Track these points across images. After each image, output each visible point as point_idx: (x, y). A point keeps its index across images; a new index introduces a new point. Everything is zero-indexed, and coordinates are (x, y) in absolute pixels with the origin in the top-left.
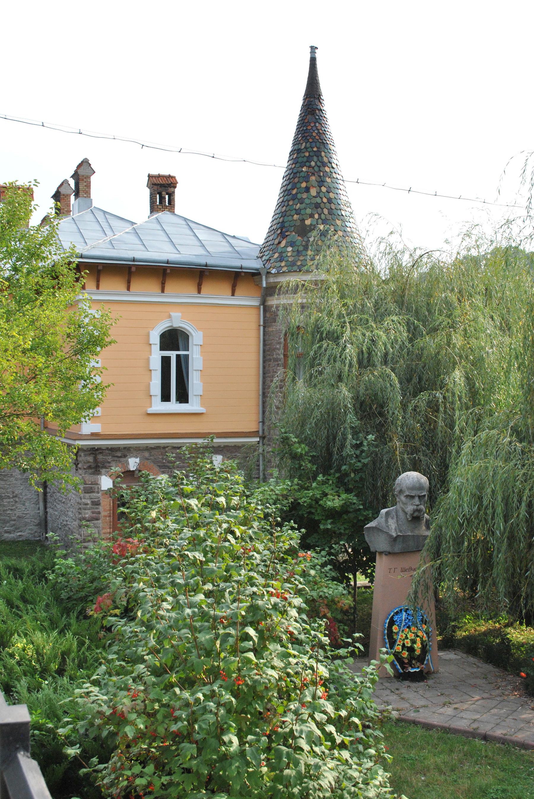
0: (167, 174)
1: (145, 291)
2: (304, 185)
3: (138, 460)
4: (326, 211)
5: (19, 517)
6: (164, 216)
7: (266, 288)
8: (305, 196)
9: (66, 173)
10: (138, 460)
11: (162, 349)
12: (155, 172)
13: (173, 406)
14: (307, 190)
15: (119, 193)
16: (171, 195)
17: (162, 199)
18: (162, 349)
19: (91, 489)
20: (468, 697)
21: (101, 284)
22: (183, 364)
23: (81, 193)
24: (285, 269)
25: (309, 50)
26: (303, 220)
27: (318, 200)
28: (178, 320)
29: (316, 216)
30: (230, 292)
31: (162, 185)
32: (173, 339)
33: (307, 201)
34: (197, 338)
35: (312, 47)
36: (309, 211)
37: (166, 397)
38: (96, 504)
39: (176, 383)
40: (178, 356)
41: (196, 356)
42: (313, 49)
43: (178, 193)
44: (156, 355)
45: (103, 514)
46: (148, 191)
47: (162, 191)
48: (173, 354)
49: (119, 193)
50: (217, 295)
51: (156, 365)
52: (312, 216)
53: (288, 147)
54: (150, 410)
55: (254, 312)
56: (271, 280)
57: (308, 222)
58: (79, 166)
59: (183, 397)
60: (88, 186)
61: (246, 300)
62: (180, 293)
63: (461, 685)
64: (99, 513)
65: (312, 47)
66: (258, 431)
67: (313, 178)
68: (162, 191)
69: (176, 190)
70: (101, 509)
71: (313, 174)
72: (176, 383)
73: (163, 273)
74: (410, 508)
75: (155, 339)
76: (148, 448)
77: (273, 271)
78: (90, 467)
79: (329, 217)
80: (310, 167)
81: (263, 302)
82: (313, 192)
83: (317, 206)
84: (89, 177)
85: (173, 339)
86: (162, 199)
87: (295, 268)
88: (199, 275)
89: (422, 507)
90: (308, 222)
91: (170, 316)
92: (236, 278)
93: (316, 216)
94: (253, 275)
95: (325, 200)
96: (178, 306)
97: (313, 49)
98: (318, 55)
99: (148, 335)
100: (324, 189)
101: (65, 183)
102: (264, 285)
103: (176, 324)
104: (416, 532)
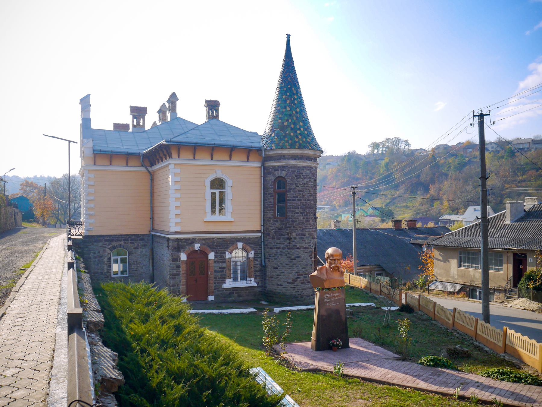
3: (199, 245)
4: (295, 118)
5: (140, 274)
7: (265, 157)
9: (164, 99)
10: (199, 245)
11: (211, 189)
12: (209, 99)
16: (217, 111)
18: (211, 189)
19: (176, 259)
20: (533, 161)
21: (214, 156)
24: (273, 147)
25: (286, 36)
26: (283, 123)
28: (219, 174)
29: (290, 121)
30: (109, 164)
31: (212, 106)
34: (229, 183)
35: (287, 35)
36: (286, 118)
38: (178, 267)
40: (219, 192)
42: (288, 36)
43: (221, 109)
44: (208, 192)
45: (181, 272)
48: (217, 191)
51: (209, 197)
52: (288, 120)
55: (259, 169)
56: (267, 153)
63: (369, 359)
64: (180, 272)
65: (287, 35)
66: (261, 230)
69: (220, 108)
70: (181, 269)
71: (288, 99)
75: (208, 184)
76: (204, 239)
78: (175, 248)
80: (287, 95)
81: (263, 165)
84: (176, 102)
85: (218, 184)
87: (279, 147)
88: (231, 150)
91: (216, 172)
92: (249, 152)
93: (290, 121)
94: (258, 150)
95: (294, 112)
96: (220, 167)
97: (288, 36)
98: (291, 38)
101: (164, 104)
102: (263, 156)
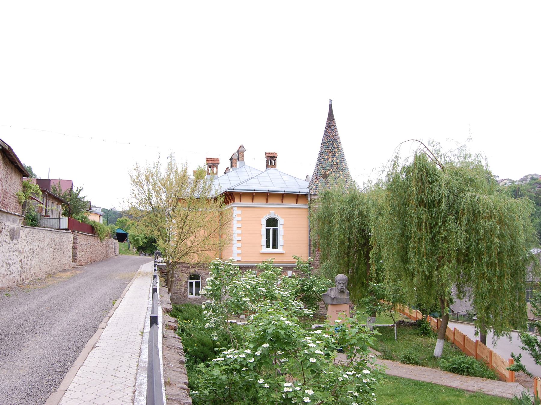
0: (273, 152)
1: (260, 203)
2: (326, 157)
4: (335, 168)
6: (271, 171)
8: (326, 162)
12: (268, 152)
13: (271, 250)
14: (328, 159)
15: (255, 160)
17: (271, 162)
22: (275, 231)
23: (240, 159)
27: (332, 163)
28: (273, 214)
29: (331, 170)
31: (271, 157)
32: (272, 222)
33: (327, 164)
34: (281, 222)
36: (328, 168)
37: (268, 246)
39: (272, 240)
41: (280, 229)
42: (331, 101)
44: (264, 228)
46: (265, 159)
47: (271, 159)
48: (272, 228)
49: (255, 160)
50: (290, 204)
51: (264, 232)
52: (329, 170)
53: (321, 141)
54: (262, 251)
57: (327, 173)
58: (239, 148)
59: (275, 246)
60: (243, 156)
61: (301, 205)
62: (274, 203)
67: (330, 154)
68: (271, 159)
72: (272, 240)
73: (267, 196)
74: (339, 287)
77: (313, 194)
79: (337, 170)
82: (330, 160)
83: (332, 166)
84: (243, 152)
85: (272, 222)
86: (271, 162)
88: (282, 196)
89: (344, 287)
90: (327, 173)
92: (298, 197)
93: (331, 170)
94: (305, 195)
95: (335, 163)
96: (273, 209)
97: (331, 101)
99: (261, 221)
100: (335, 159)
103: (272, 216)
104: (342, 297)
